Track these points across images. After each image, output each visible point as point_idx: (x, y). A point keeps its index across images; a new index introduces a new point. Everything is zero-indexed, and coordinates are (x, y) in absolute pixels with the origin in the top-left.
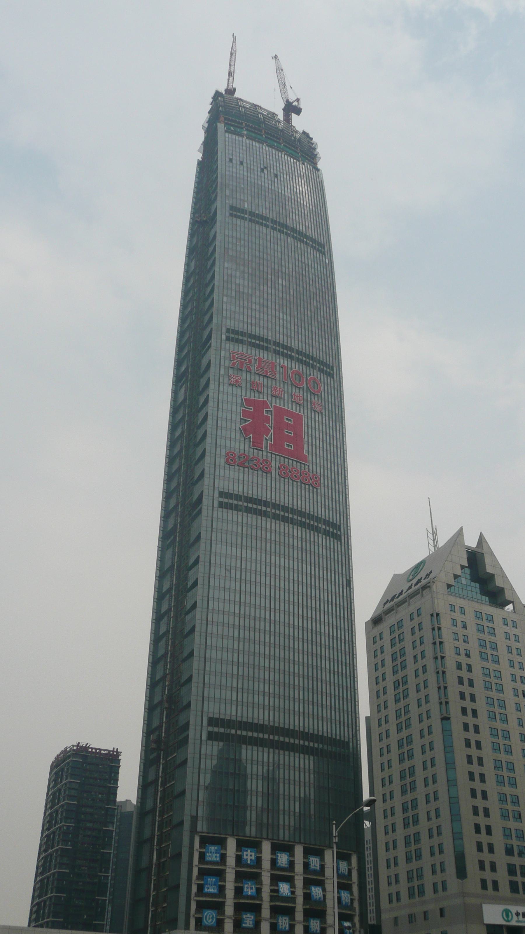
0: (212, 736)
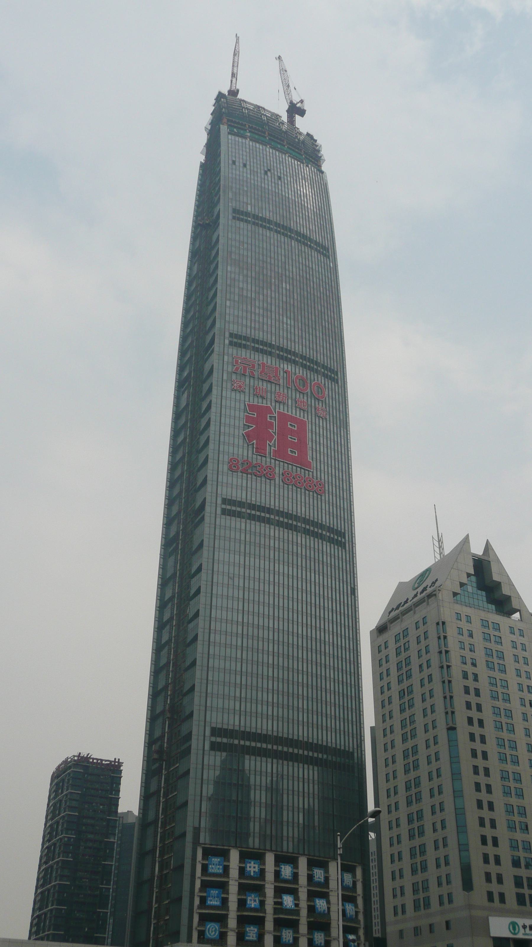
0: (214, 747)
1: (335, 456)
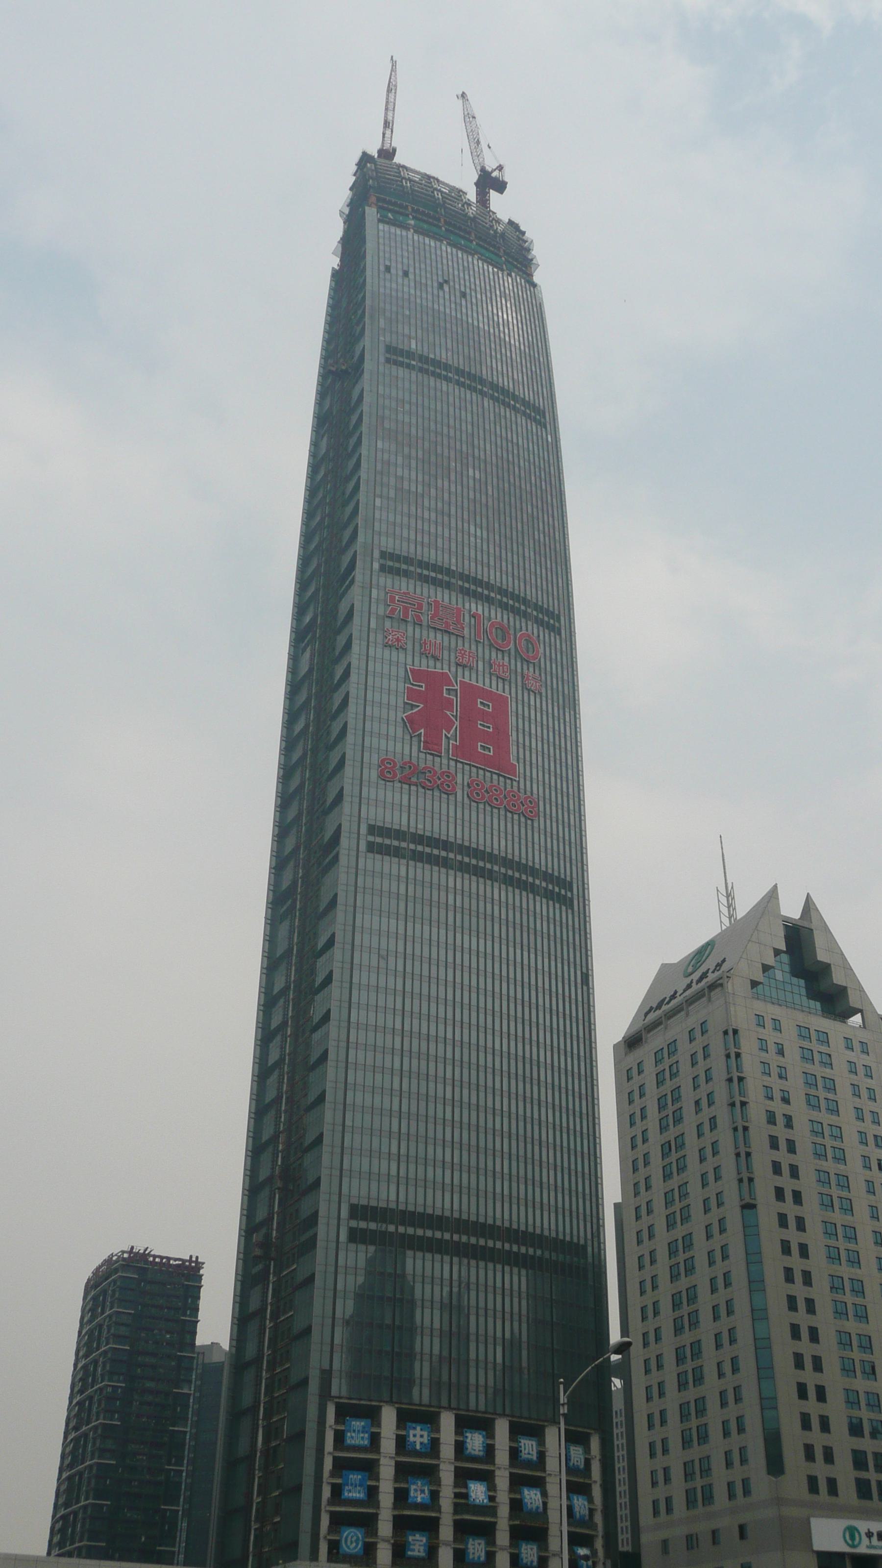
0: (355, 1236)
1: (555, 755)
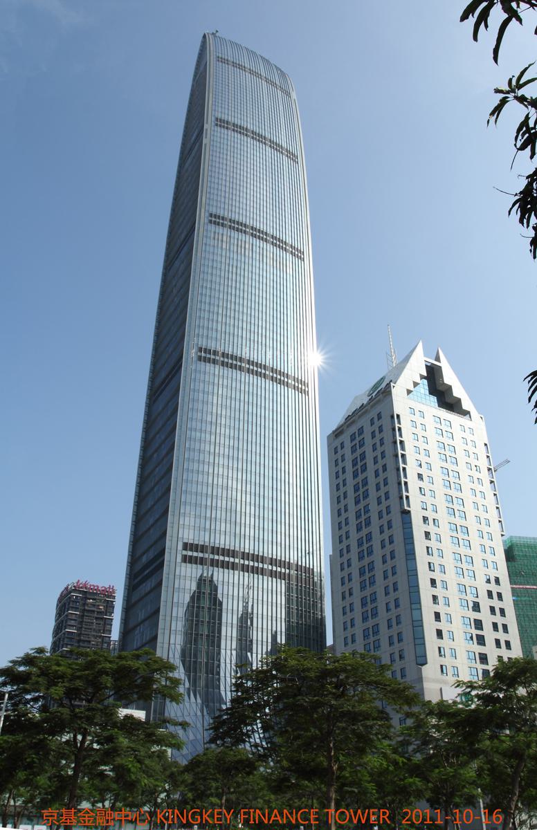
0: (186, 559)
